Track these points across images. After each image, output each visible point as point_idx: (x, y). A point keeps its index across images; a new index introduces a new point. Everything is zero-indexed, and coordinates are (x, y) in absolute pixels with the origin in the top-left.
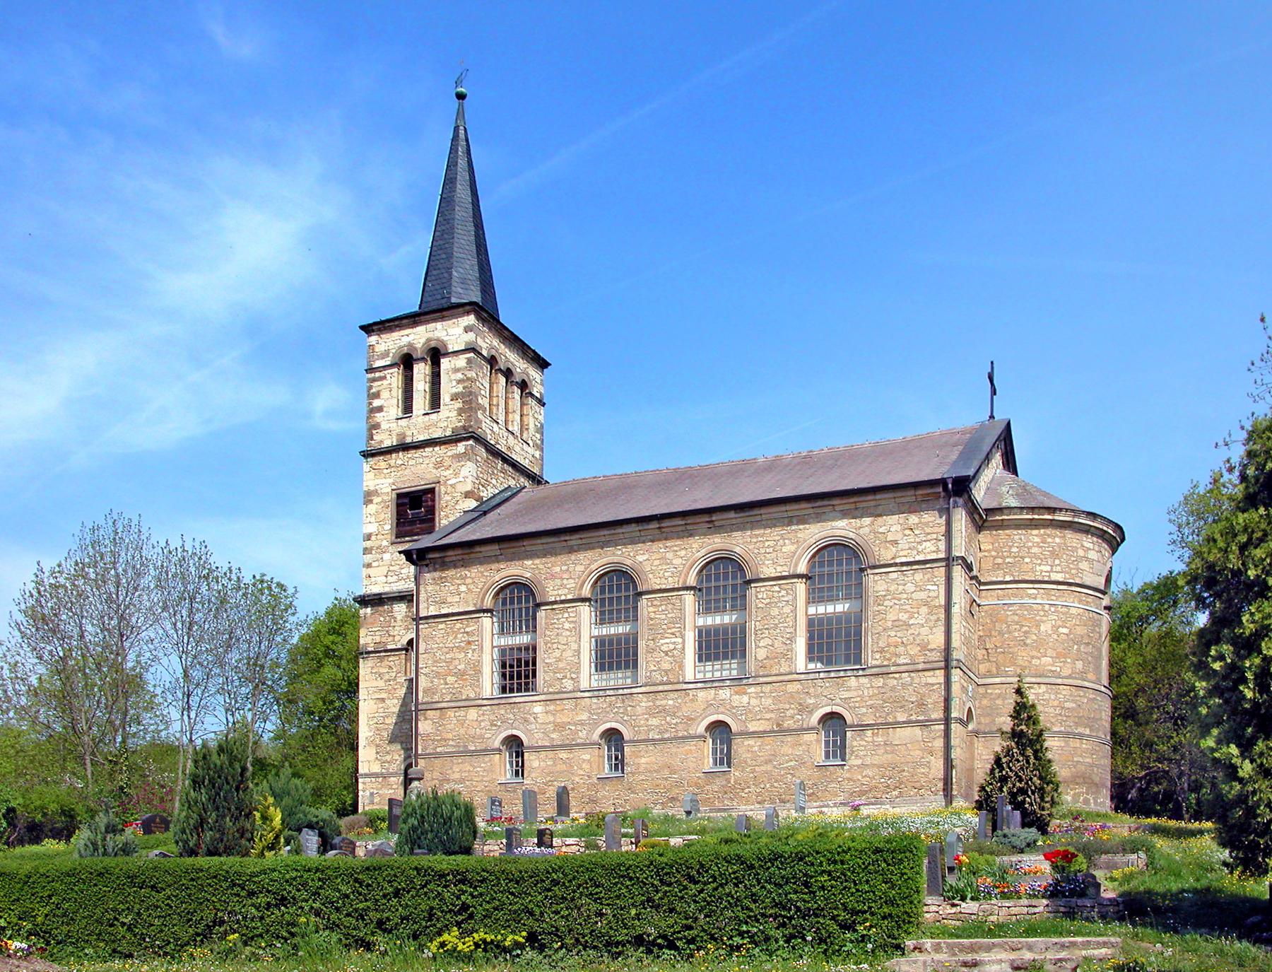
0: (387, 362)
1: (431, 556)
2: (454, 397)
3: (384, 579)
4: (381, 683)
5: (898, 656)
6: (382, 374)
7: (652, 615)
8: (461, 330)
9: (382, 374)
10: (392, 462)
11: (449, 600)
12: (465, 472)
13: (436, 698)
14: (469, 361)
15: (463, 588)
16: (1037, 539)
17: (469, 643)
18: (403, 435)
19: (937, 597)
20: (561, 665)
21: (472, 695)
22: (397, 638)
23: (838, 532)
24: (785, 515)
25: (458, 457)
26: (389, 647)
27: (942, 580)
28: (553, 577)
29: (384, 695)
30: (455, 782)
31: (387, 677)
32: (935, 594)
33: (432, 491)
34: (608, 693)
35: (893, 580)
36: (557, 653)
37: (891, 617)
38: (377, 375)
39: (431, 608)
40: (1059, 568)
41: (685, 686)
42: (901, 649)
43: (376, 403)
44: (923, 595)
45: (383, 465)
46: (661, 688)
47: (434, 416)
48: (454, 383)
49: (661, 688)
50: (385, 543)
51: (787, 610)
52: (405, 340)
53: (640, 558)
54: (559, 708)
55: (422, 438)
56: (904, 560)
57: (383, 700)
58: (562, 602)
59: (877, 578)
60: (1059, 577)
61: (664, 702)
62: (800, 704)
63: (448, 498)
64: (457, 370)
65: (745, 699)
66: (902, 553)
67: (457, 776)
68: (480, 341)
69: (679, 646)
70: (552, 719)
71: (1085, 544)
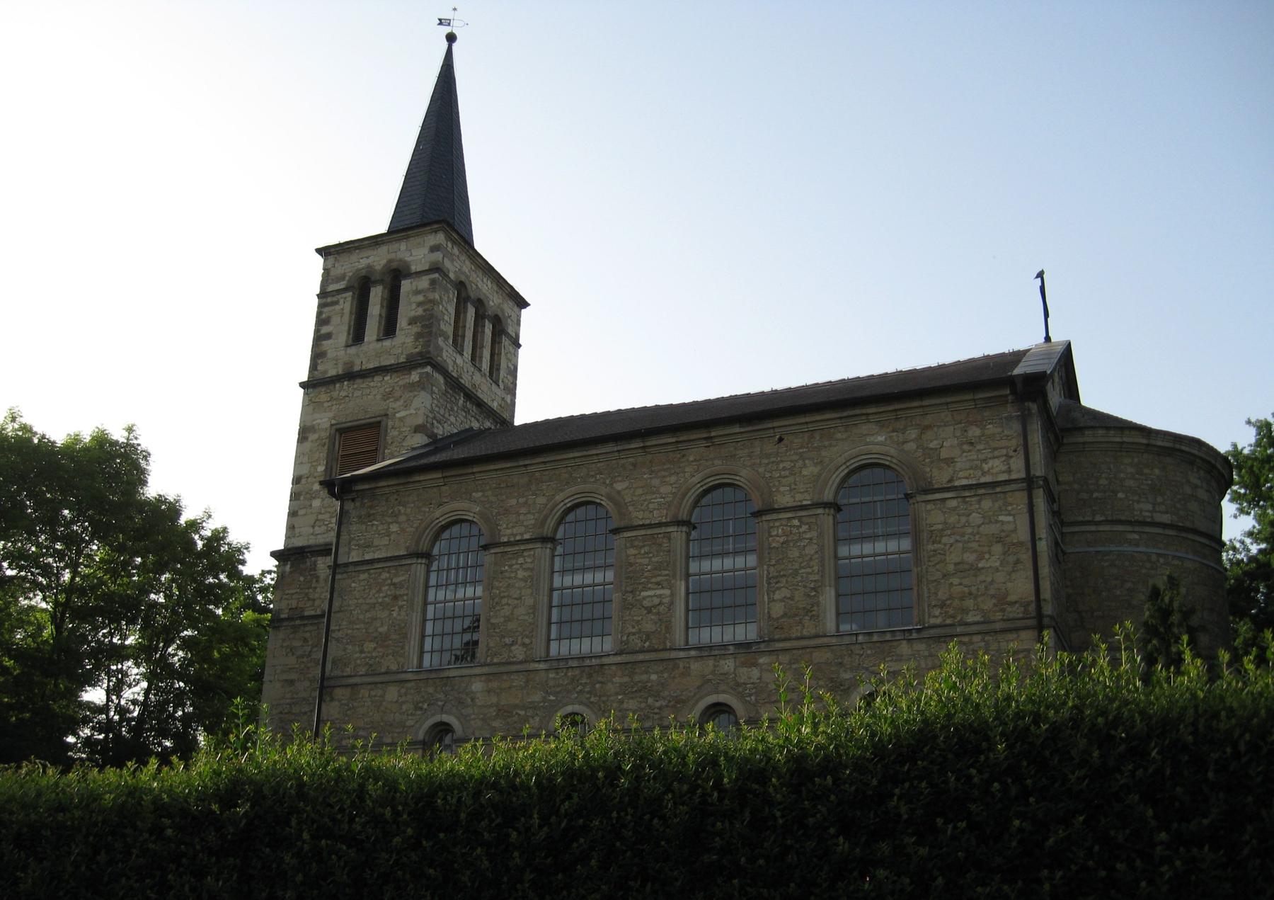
0: (342, 285)
1: (360, 487)
2: (412, 321)
3: (311, 530)
5: (965, 611)
6: (335, 299)
7: (632, 560)
8: (426, 250)
9: (335, 299)
10: (335, 394)
11: (376, 542)
12: (417, 403)
13: (348, 671)
14: (433, 282)
15: (394, 528)
16: (1130, 470)
17: (395, 598)
18: (352, 364)
19: (1015, 531)
20: (511, 626)
21: (394, 667)
22: (317, 603)
25: (412, 387)
26: (306, 614)
27: (1023, 507)
29: (293, 676)
31: (299, 653)
32: (1011, 527)
34: (571, 663)
35: (955, 509)
36: (506, 611)
37: (953, 557)
38: (329, 300)
39: (354, 553)
40: (1163, 508)
41: (673, 655)
42: (969, 603)
44: (993, 529)
45: (324, 397)
46: (641, 657)
47: (387, 343)
48: (414, 306)
49: (641, 657)
51: (811, 550)
52: (364, 262)
53: (619, 486)
55: (371, 366)
56: (965, 482)
57: (292, 682)
58: (517, 543)
59: (929, 507)
60: (1166, 518)
61: (644, 677)
62: (831, 680)
63: (396, 433)
64: (417, 292)
65: (755, 672)
66: (961, 474)
68: (447, 264)
69: (666, 600)
70: (494, 699)
71: (1192, 479)
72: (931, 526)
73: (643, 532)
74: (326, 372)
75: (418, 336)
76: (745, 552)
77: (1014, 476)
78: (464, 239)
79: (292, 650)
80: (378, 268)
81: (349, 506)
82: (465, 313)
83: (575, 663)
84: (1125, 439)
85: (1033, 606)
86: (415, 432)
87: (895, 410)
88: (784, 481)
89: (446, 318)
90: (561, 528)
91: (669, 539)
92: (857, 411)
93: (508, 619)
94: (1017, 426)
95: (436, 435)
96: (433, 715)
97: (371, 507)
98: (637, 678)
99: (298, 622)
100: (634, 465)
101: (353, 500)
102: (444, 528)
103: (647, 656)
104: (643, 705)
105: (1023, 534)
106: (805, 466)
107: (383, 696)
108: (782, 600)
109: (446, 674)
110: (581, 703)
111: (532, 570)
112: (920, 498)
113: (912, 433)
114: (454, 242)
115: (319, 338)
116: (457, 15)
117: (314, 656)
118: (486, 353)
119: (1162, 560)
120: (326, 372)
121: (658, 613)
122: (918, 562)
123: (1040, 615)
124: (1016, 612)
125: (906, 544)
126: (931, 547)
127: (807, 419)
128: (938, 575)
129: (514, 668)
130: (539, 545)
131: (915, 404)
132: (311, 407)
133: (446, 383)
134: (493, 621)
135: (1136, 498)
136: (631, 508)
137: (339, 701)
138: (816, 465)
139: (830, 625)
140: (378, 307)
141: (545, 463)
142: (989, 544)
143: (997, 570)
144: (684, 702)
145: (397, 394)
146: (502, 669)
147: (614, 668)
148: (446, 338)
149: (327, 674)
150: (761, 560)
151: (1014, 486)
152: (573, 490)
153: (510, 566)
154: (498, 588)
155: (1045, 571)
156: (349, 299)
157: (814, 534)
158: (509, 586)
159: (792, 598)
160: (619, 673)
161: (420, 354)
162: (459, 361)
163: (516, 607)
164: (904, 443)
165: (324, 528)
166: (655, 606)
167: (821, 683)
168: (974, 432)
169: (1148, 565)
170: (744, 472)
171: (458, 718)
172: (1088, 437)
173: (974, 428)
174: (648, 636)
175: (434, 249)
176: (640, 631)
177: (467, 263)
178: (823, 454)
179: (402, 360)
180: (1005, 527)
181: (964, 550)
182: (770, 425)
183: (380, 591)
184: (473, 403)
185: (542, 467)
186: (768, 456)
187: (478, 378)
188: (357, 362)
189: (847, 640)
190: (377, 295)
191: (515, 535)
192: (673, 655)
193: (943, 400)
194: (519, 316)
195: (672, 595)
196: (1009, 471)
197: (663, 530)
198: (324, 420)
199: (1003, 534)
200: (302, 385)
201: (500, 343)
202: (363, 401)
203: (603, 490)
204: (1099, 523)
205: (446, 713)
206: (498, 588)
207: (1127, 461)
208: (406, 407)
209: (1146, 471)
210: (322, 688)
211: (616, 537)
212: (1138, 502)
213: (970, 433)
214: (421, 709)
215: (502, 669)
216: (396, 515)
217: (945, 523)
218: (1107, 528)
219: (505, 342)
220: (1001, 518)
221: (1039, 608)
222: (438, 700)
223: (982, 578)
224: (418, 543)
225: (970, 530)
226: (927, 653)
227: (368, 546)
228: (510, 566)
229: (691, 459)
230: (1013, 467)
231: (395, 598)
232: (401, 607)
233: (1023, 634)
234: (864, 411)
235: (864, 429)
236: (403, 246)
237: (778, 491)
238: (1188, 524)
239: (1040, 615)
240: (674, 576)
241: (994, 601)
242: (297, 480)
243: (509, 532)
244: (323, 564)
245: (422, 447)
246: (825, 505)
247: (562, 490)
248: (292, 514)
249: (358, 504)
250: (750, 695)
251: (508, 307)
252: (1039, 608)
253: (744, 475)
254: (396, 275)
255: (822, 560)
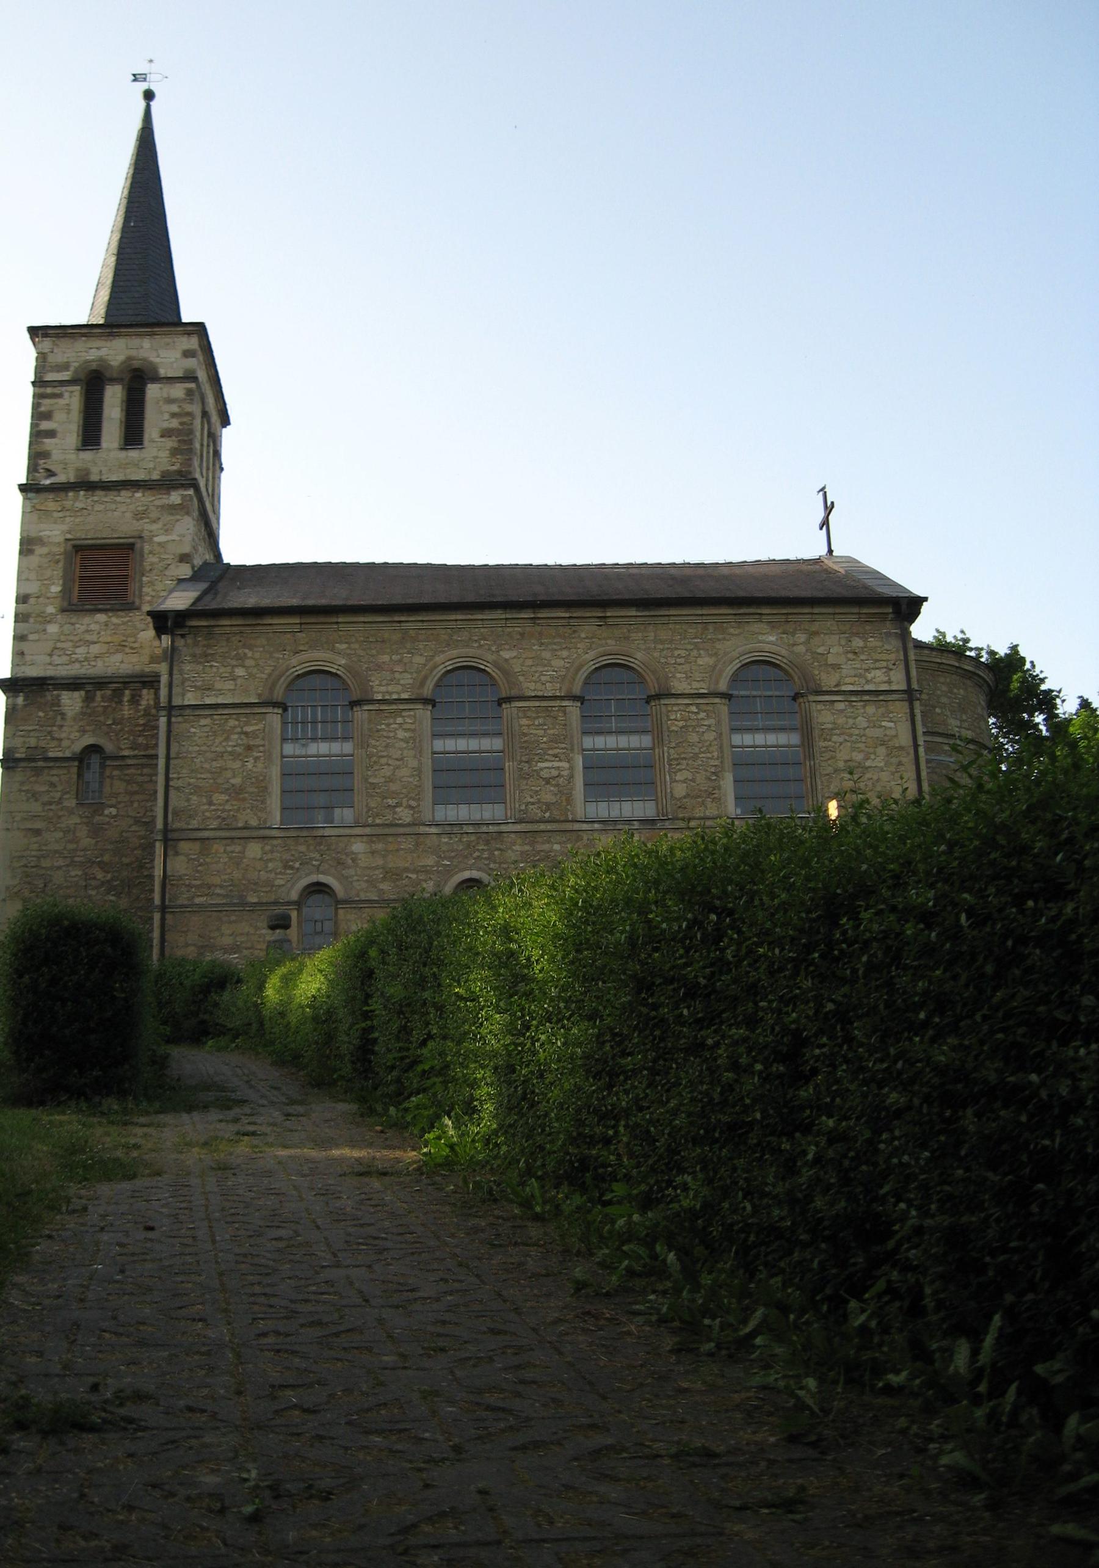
0: (65, 376)
2: (166, 433)
3: (47, 659)
4: (36, 807)
6: (57, 390)
8: (179, 355)
9: (57, 390)
10: (68, 504)
11: (218, 686)
13: (194, 824)
14: (189, 393)
15: (240, 672)
16: (944, 688)
17: (249, 748)
19: (896, 736)
21: (254, 822)
22: (65, 743)
23: (767, 647)
24: (699, 620)
26: (51, 755)
28: (379, 667)
29: (38, 825)
30: (226, 950)
31: (45, 798)
32: (893, 733)
33: (131, 547)
34: (466, 829)
35: (842, 711)
36: (387, 771)
37: (843, 755)
38: (49, 390)
39: (189, 695)
40: (966, 725)
41: (577, 826)
43: (45, 425)
44: (877, 733)
45: (51, 505)
46: (542, 827)
47: (133, 454)
48: (166, 416)
49: (542, 827)
50: (51, 609)
51: (710, 736)
52: (93, 355)
53: (506, 655)
54: (391, 847)
57: (37, 832)
59: (819, 707)
61: (546, 847)
63: (155, 559)
64: (170, 401)
66: (847, 680)
67: (227, 941)
69: (565, 773)
70: (380, 862)
73: (537, 704)
75: (174, 452)
77: (894, 688)
79: (35, 796)
81: (180, 642)
83: (471, 829)
87: (787, 614)
88: (679, 667)
91: (565, 713)
92: (752, 610)
93: (390, 780)
96: (307, 875)
97: (208, 646)
99: (40, 764)
100: (522, 635)
103: (549, 827)
105: (905, 739)
106: (700, 656)
107: (243, 852)
108: (684, 782)
109: (320, 833)
111: (413, 731)
112: (812, 698)
113: (801, 637)
115: (37, 435)
116: (154, 67)
117: (66, 803)
121: (558, 785)
122: (811, 756)
126: (822, 744)
128: (830, 770)
129: (402, 830)
130: (420, 706)
134: (371, 780)
137: (187, 855)
138: (711, 656)
141: (423, 621)
145: (154, 515)
146: (387, 831)
147: (513, 836)
152: (455, 653)
153: (388, 725)
154: (375, 747)
156: (77, 394)
158: (387, 746)
159: (693, 780)
160: (519, 841)
163: (398, 767)
164: (794, 645)
165: (65, 659)
166: (554, 778)
168: (858, 643)
173: (858, 639)
174: (548, 806)
176: (539, 801)
178: (718, 646)
180: (888, 732)
181: (853, 749)
186: (662, 642)
190: (114, 399)
191: (391, 693)
192: (577, 826)
193: (830, 610)
196: (889, 682)
197: (558, 703)
198: (56, 533)
199: (886, 738)
200: (23, 488)
205: (323, 873)
206: (375, 747)
207: (942, 680)
208: (167, 531)
214: (292, 868)
215: (387, 831)
216: (241, 658)
217: (834, 723)
220: (883, 724)
222: (311, 859)
224: (272, 690)
225: (857, 732)
227: (208, 689)
228: (388, 725)
229: (583, 635)
230: (893, 679)
231: (249, 748)
232: (256, 759)
234: (759, 611)
235: (756, 627)
236: (146, 343)
240: (572, 750)
242: (22, 599)
243: (383, 689)
248: (19, 638)
249: (190, 641)
253: (639, 657)
254: (138, 379)
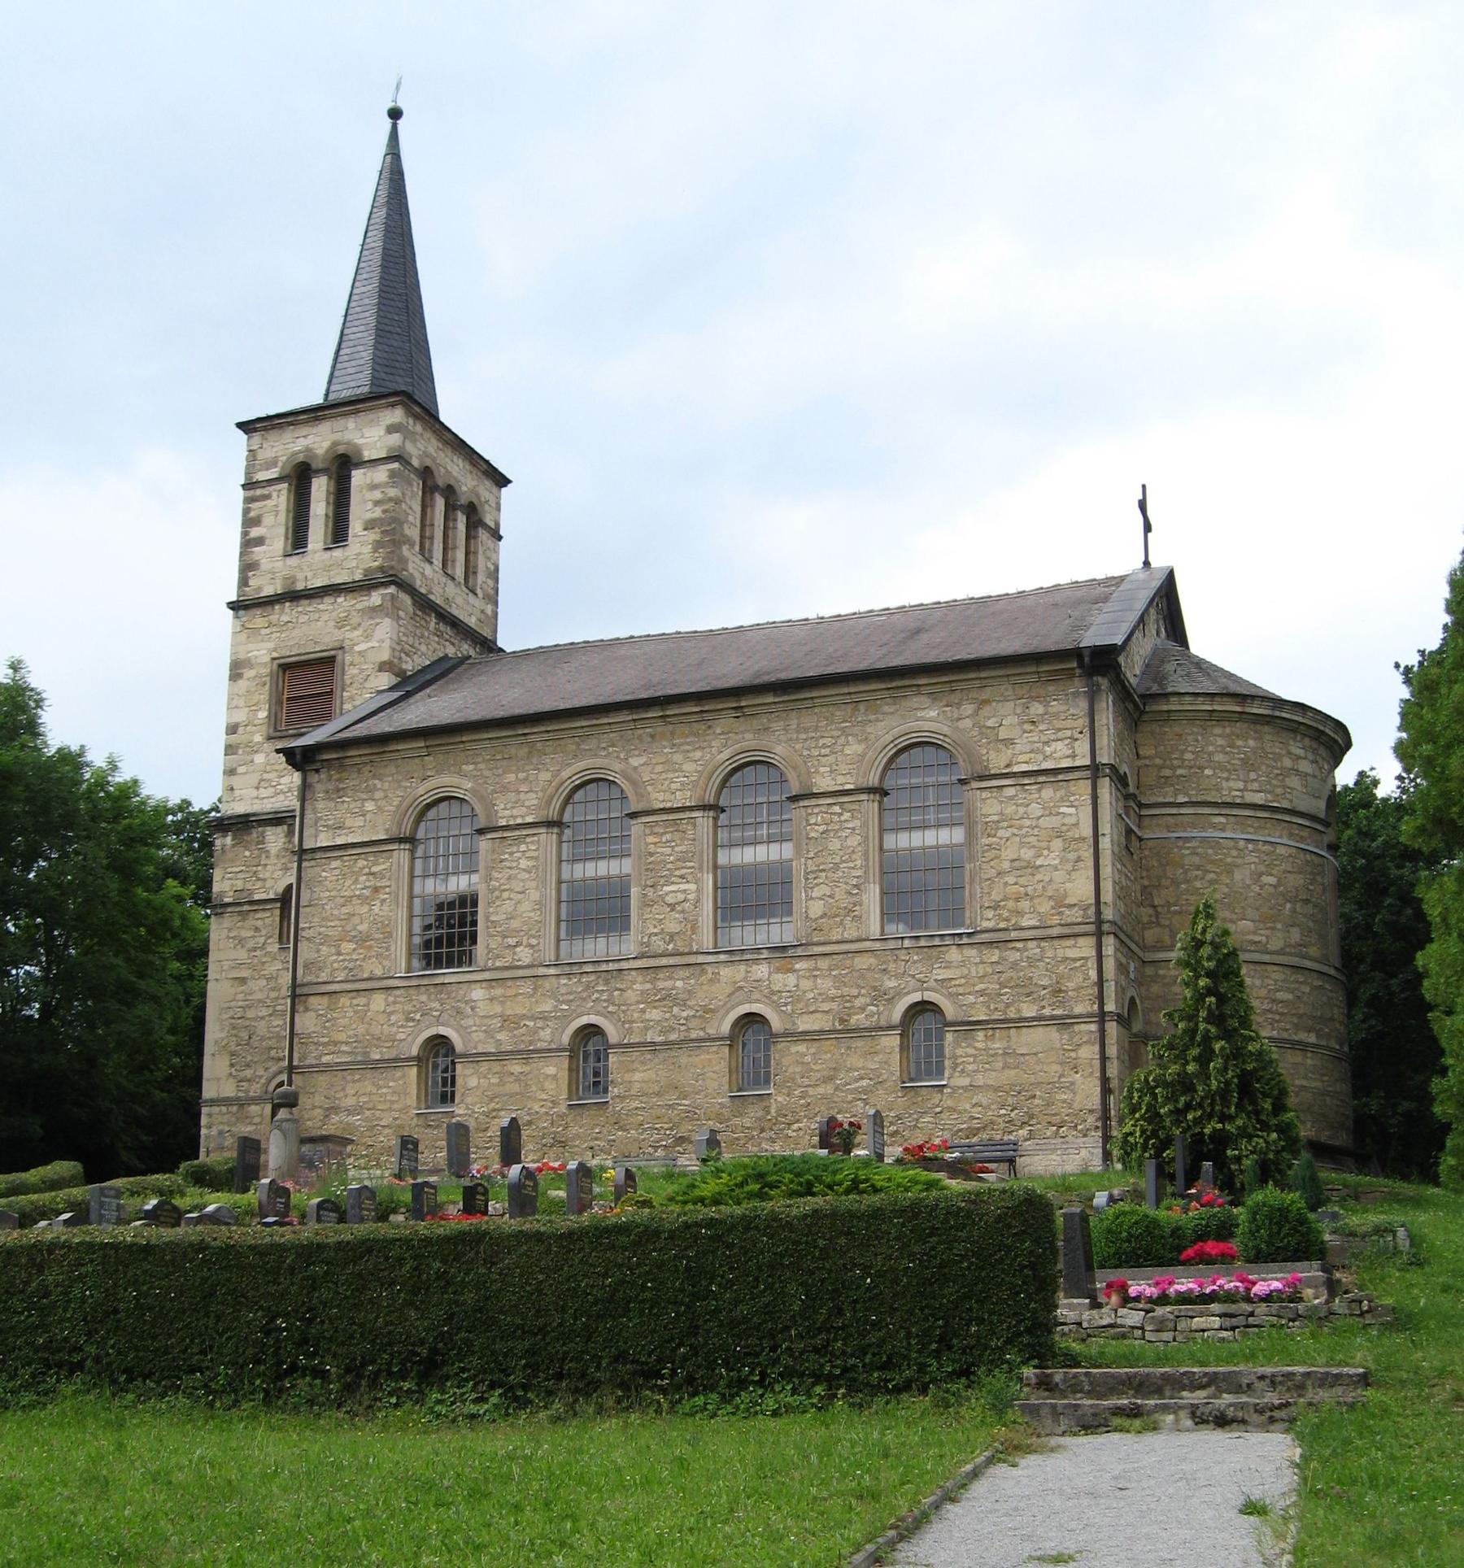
2: (369, 526)
3: (255, 793)
5: (1019, 913)
6: (265, 491)
10: (274, 618)
11: (348, 823)
13: (323, 977)
14: (393, 474)
15: (370, 806)
17: (376, 890)
18: (294, 580)
19: (1076, 825)
20: (515, 924)
21: (378, 972)
22: (269, 884)
26: (256, 897)
27: (1087, 798)
31: (251, 944)
32: (1073, 820)
35: (1011, 798)
36: (508, 906)
37: (1009, 853)
38: (258, 492)
39: (322, 836)
40: (1255, 786)
41: (701, 959)
42: (1025, 905)
45: (259, 622)
46: (664, 961)
47: (337, 553)
48: (370, 505)
49: (664, 961)
51: (854, 841)
52: (299, 445)
56: (1024, 768)
59: (985, 794)
60: (1259, 798)
61: (669, 984)
62: (875, 989)
63: (355, 671)
64: (373, 487)
65: (791, 979)
66: (1022, 758)
70: (498, 1009)
72: (986, 816)
73: (665, 817)
74: (260, 589)
75: (377, 545)
76: (782, 839)
78: (425, 412)
79: (241, 942)
80: (320, 452)
82: (433, 506)
84: (1216, 707)
85: (1092, 909)
86: (380, 671)
89: (411, 518)
90: (569, 808)
91: (695, 826)
94: (1083, 704)
95: (405, 671)
97: (339, 780)
98: (661, 985)
99: (246, 908)
101: (317, 771)
102: (429, 806)
103: (671, 961)
104: (668, 1015)
105: (1087, 830)
107: (368, 1005)
110: (598, 1013)
111: (536, 858)
112: (975, 785)
113: (968, 709)
114: (416, 417)
118: (460, 555)
119: (1250, 846)
120: (260, 589)
123: (1099, 921)
124: (1074, 915)
125: (958, 835)
126: (986, 841)
127: (852, 690)
129: (520, 973)
130: (543, 830)
131: (972, 675)
132: (243, 636)
133: (415, 603)
135: (1225, 775)
136: (649, 788)
138: (860, 742)
139: (874, 928)
140: (323, 504)
142: (1041, 839)
143: (1056, 869)
144: (713, 1011)
145: (355, 620)
146: (506, 974)
147: (633, 973)
148: (412, 545)
149: (299, 981)
150: (798, 850)
151: (1077, 775)
153: (511, 854)
155: (1107, 871)
156: (285, 492)
157: (857, 823)
158: (509, 878)
160: (640, 979)
161: (381, 569)
162: (428, 570)
167: (863, 991)
168: (1037, 709)
169: (1234, 853)
170: (779, 749)
171: (457, 1031)
172: (1173, 705)
173: (1037, 705)
174: (672, 936)
175: (391, 429)
177: (434, 441)
178: (869, 730)
179: (358, 577)
180: (1067, 820)
181: (1022, 844)
182: (808, 695)
183: (356, 882)
184: (446, 623)
185: (546, 736)
186: (806, 730)
187: (451, 590)
188: (300, 576)
189: (891, 945)
190: (320, 488)
192: (701, 959)
194: (498, 498)
195: (698, 890)
197: (687, 814)
198: (263, 653)
199: (1064, 828)
200: (233, 606)
201: (476, 537)
202: (309, 630)
203: (617, 766)
204: (1181, 805)
207: (1218, 731)
208: (368, 637)
209: (1239, 743)
210: (294, 996)
211: (633, 822)
212: (1228, 779)
213: (1032, 711)
215: (506, 974)
217: (1001, 814)
218: (1191, 810)
219: (483, 535)
220: (1062, 810)
221: (1098, 913)
223: (1038, 877)
225: (1028, 823)
226: (978, 960)
228: (511, 854)
229: (718, 731)
231: (376, 890)
233: (1081, 941)
235: (915, 701)
237: (816, 772)
238: (1285, 804)
239: (1099, 921)
240: (701, 868)
241: (1052, 903)
243: (508, 813)
244: (275, 838)
245: (391, 689)
246: (870, 790)
247: (569, 765)
250: (786, 1005)
251: (485, 489)
252: (1098, 913)
253: (780, 751)
254: (343, 465)
255: (866, 854)
